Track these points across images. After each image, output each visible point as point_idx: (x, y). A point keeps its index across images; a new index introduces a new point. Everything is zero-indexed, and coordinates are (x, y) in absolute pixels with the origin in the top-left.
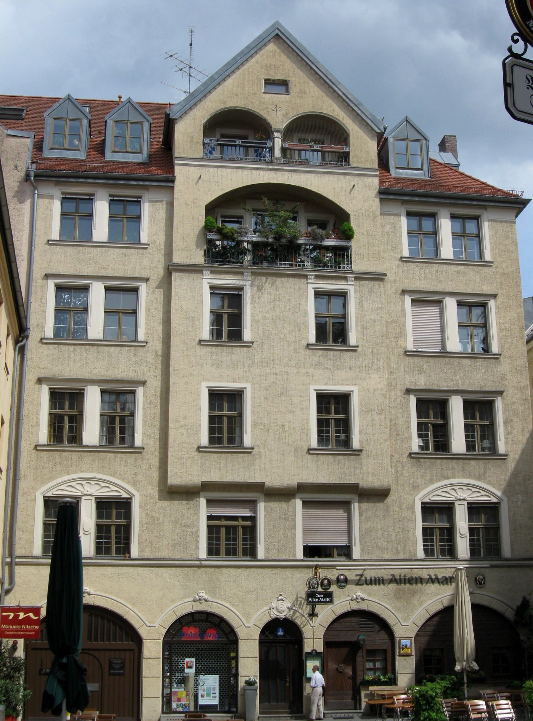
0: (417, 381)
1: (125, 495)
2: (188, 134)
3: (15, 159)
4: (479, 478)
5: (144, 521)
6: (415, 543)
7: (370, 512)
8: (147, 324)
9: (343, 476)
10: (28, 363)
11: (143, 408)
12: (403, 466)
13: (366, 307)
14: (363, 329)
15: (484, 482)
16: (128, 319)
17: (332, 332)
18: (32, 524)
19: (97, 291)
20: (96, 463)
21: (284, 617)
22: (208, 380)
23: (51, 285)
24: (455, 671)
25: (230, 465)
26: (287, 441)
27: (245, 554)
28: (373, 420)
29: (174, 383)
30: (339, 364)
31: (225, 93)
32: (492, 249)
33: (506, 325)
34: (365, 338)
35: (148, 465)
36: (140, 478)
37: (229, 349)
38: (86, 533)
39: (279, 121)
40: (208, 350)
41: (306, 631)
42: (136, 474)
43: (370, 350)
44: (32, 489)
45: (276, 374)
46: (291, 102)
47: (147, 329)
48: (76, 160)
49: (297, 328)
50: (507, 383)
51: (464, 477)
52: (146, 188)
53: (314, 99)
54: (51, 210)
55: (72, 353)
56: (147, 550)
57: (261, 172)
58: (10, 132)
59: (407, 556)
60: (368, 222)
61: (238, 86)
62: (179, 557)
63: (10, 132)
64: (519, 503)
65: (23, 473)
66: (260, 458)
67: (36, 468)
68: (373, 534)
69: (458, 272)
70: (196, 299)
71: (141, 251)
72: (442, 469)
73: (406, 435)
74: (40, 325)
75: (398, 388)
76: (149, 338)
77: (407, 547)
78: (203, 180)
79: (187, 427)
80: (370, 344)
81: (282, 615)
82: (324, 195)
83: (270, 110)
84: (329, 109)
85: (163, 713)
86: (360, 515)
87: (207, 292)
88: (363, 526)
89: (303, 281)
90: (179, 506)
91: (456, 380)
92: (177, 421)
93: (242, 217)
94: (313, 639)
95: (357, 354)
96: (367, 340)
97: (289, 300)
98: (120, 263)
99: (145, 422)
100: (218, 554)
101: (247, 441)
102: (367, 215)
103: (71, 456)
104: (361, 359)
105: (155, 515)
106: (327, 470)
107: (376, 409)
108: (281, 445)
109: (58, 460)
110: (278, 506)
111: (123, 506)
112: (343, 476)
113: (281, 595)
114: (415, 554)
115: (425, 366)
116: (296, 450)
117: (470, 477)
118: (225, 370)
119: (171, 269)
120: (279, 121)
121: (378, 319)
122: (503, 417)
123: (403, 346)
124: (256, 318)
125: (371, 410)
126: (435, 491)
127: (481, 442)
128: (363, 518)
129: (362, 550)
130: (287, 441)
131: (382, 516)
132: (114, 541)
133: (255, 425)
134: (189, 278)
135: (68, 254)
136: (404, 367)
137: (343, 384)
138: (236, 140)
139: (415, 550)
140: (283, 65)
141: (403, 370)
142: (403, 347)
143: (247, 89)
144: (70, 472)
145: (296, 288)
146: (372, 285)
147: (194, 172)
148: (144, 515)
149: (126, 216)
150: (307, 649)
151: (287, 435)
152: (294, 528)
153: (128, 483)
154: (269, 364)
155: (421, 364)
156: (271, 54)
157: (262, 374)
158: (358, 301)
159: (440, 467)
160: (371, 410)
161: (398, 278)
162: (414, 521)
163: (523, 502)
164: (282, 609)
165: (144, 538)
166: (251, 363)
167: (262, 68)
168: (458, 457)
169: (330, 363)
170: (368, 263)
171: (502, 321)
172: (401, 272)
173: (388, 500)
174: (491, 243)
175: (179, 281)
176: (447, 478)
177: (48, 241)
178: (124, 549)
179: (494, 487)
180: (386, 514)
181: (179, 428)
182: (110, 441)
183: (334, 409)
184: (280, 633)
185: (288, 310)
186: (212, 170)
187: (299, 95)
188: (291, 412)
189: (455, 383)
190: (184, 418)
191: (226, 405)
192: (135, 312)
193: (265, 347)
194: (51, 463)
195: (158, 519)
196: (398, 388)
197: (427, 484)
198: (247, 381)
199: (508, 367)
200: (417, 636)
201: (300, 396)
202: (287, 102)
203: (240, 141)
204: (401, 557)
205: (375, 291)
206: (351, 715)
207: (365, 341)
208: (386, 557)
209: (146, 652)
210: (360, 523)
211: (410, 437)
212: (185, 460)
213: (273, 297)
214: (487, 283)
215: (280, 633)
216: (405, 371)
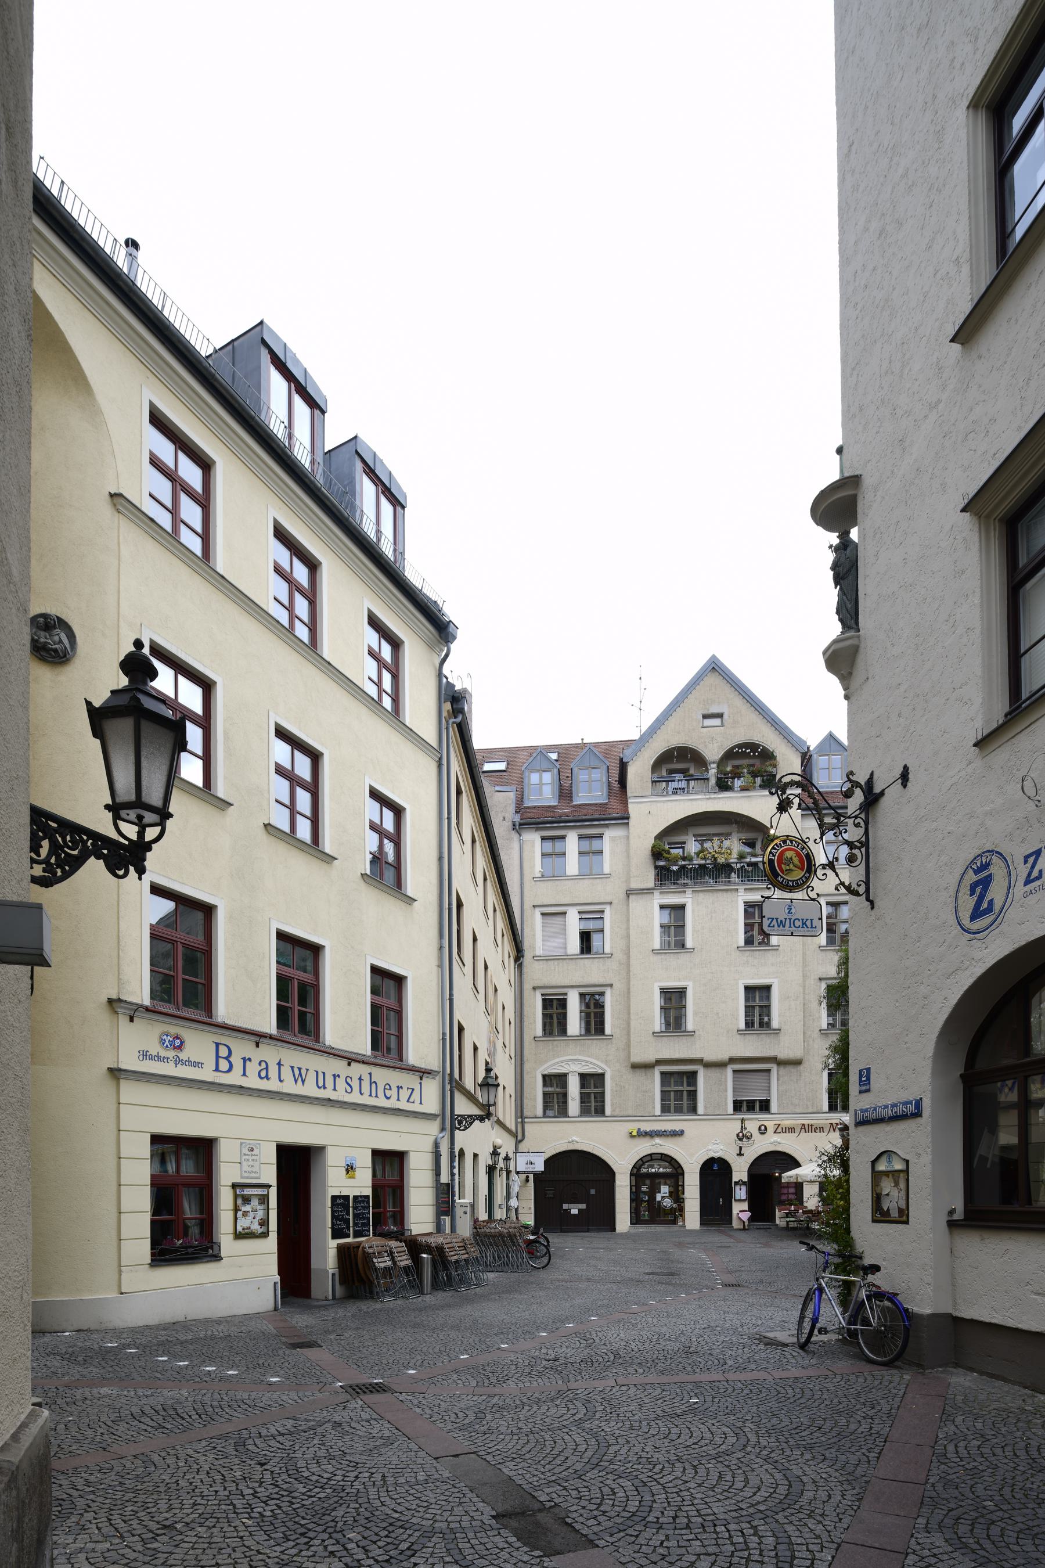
1: (600, 1071)
2: (639, 772)
8: (611, 939)
10: (525, 976)
16: (558, 860)
23: (538, 912)
24: (130, 682)
27: (688, 1111)
37: (676, 955)
38: (573, 1099)
39: (713, 752)
40: (659, 957)
42: (607, 1055)
48: (550, 806)
52: (607, 826)
57: (700, 802)
58: (497, 788)
59: (815, 1110)
63: (497, 788)
70: (649, 914)
71: (604, 880)
78: (653, 811)
81: (716, 1155)
87: (657, 993)
89: (734, 894)
90: (640, 1076)
93: (684, 843)
94: (740, 1173)
98: (589, 891)
99: (612, 1016)
100: (669, 1111)
101: (690, 1027)
103: (558, 1042)
106: (753, 1046)
108: (716, 1030)
110: (714, 1073)
111: (599, 1078)
118: (673, 972)
119: (629, 893)
120: (713, 752)
129: (779, 1106)
132: (593, 1104)
133: (695, 1014)
147: (645, 808)
149: (590, 854)
150: (735, 1179)
173: (801, 1067)
175: (636, 902)
178: (600, 1111)
182: (588, 1031)
184: (716, 1168)
186: (659, 804)
191: (674, 1000)
192: (602, 931)
208: (798, 1111)
209: (618, 1182)
211: (820, 1017)
215: (716, 1168)
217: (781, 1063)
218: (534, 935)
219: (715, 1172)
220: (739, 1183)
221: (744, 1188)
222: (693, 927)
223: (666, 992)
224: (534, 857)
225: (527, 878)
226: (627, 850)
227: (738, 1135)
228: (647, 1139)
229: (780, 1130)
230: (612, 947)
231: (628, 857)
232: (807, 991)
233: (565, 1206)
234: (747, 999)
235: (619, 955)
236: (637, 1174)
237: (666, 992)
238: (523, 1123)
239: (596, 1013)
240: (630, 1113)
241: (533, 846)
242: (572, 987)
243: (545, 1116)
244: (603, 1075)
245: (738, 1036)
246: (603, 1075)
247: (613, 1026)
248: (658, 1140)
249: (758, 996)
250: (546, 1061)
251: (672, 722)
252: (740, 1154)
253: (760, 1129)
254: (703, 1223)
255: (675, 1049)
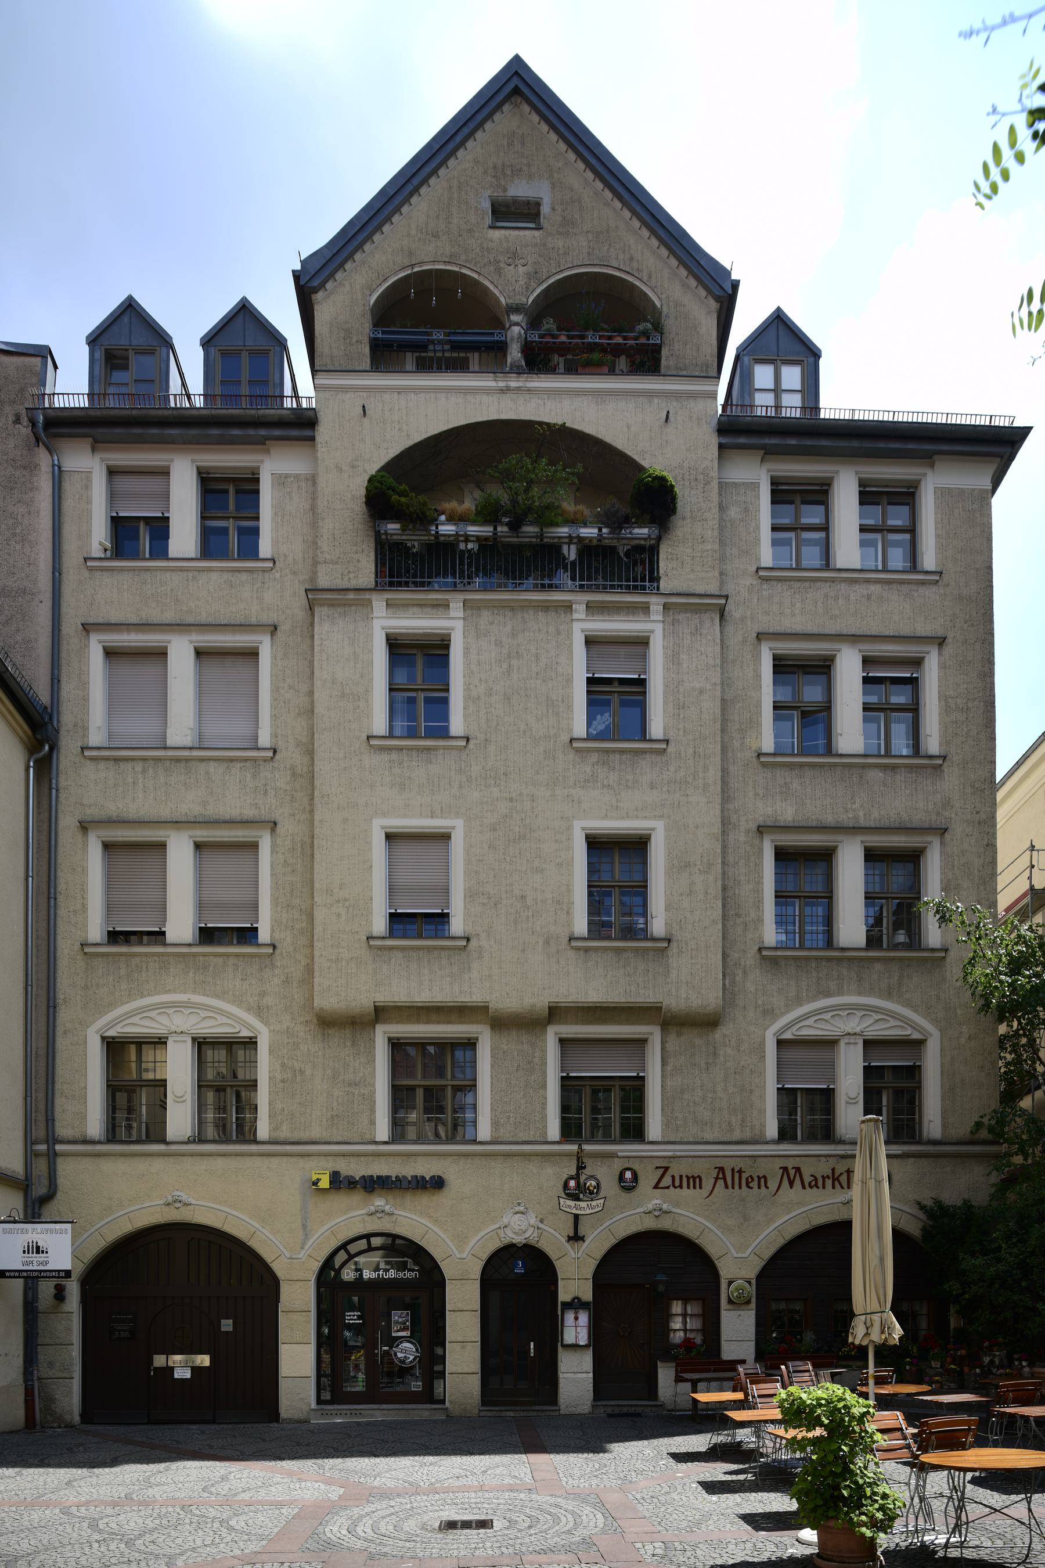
0: (779, 812)
3: (14, 402)
4: (888, 995)
5: (279, 1076)
6: (762, 1112)
7: (683, 1057)
8: (274, 717)
9: (633, 989)
11: (272, 875)
12: (745, 972)
13: (685, 665)
14: (677, 706)
15: (898, 1002)
17: (619, 699)
18: (83, 1085)
19: (181, 653)
20: (191, 974)
21: (524, 1242)
22: (384, 815)
25: (426, 972)
26: (530, 925)
28: (692, 884)
29: (321, 821)
30: (630, 777)
31: (413, 232)
32: (941, 548)
33: (959, 701)
34: (681, 726)
35: (283, 978)
36: (269, 1000)
41: (563, 1268)
42: (263, 994)
43: (691, 750)
44: (80, 1023)
45: (511, 800)
46: (545, 245)
47: (274, 726)
49: (550, 711)
50: (953, 816)
51: (860, 994)
53: (590, 236)
54: (89, 501)
55: (140, 776)
56: (284, 1127)
59: (747, 1135)
60: (693, 492)
61: (438, 217)
62: (340, 1139)
64: (963, 1041)
65: (62, 997)
66: (480, 957)
67: (86, 987)
68: (686, 1097)
69: (869, 597)
72: (819, 978)
73: (753, 915)
74: (80, 724)
75: (742, 829)
76: (280, 743)
77: (749, 1119)
79: (347, 904)
80: (691, 737)
81: (519, 1240)
82: (608, 439)
83: (502, 265)
84: (621, 257)
85: (319, 1401)
86: (664, 1062)
88: (669, 1083)
91: (854, 810)
92: (329, 891)
95: (664, 759)
96: (685, 731)
97: (537, 657)
99: (275, 901)
102: (692, 477)
104: (672, 769)
105: (297, 1066)
107: (699, 863)
109: (123, 972)
110: (514, 1044)
112: (633, 989)
113: (519, 1204)
114: (763, 1131)
115: (795, 785)
116: (547, 942)
117: (871, 993)
121: (708, 687)
122: (941, 880)
123: (754, 746)
124: (474, 694)
125: (688, 865)
126: (805, 1016)
127: (894, 934)
128: (669, 1068)
130: (530, 925)
131: (703, 1065)
134: (347, 619)
135: (125, 587)
136: (754, 787)
137: (637, 817)
138: (435, 331)
139: (763, 1126)
140: (529, 165)
141: (752, 793)
142: (754, 748)
143: (455, 221)
144: (146, 992)
145: (550, 630)
146: (698, 621)
148: (278, 1067)
151: (530, 914)
152: (544, 1086)
153: (249, 1010)
154: (498, 782)
155: (788, 780)
156: (505, 142)
157: (485, 800)
158: (670, 653)
159: (814, 974)
160: (688, 865)
161: (749, 613)
162: (762, 1074)
163: (970, 1037)
164: (518, 1227)
165: (279, 1106)
166: (465, 779)
167: (485, 172)
168: (848, 958)
169: (613, 777)
170: (692, 576)
171: (951, 692)
172: (755, 601)
174: (937, 536)
176: (828, 994)
177: (86, 559)
178: (245, 1133)
179: (916, 1011)
180: (710, 1061)
181: (332, 905)
183: (618, 859)
185: (534, 675)
187: (561, 230)
188: (540, 871)
189: (850, 816)
190: (342, 886)
193: (492, 748)
194: (111, 978)
195: (302, 1072)
196: (742, 829)
197: (788, 1008)
198: (457, 815)
199: (957, 782)
200: (760, 1277)
201: (556, 841)
202: (536, 245)
203: (442, 331)
204: (737, 1135)
205: (704, 631)
206: (639, 1410)
207: (681, 733)
208: (709, 1136)
210: (662, 1076)
211: (760, 920)
212: (344, 963)
213: (505, 651)
214: (926, 618)
215: (519, 1269)
216: (756, 794)
217: (673, 1022)
218: (86, 699)
219: (518, 1279)
220: (576, 1304)
221: (584, 1318)
222: (467, 688)
223: (599, 846)
224: (89, 513)
225: (71, 560)
226: (311, 505)
227: (566, 1186)
228: (357, 1197)
229: (667, 1181)
230: (274, 735)
231: (314, 525)
232: (731, 859)
233: (159, 1361)
234: (592, 869)
235: (291, 756)
236: (327, 1278)
237: (599, 846)
238: (52, 1157)
239: (428, 1090)
240: (315, 1133)
241: (88, 487)
242: (177, 824)
243: (112, 1135)
244: (251, 1043)
245: (571, 954)
246: (251, 1043)
247: (276, 923)
248: (379, 1202)
249: (618, 859)
250: (112, 1006)
251: (419, 209)
252: (576, 1238)
253: (621, 1177)
254: (488, 1395)
255: (416, 980)
